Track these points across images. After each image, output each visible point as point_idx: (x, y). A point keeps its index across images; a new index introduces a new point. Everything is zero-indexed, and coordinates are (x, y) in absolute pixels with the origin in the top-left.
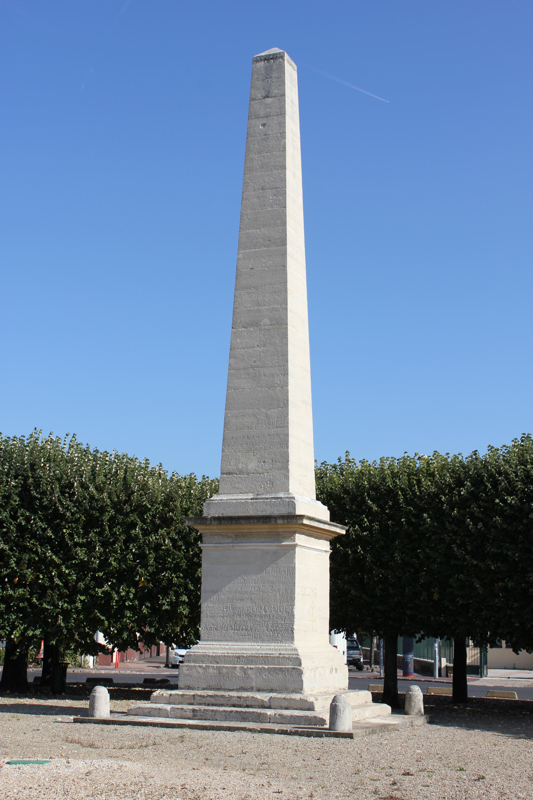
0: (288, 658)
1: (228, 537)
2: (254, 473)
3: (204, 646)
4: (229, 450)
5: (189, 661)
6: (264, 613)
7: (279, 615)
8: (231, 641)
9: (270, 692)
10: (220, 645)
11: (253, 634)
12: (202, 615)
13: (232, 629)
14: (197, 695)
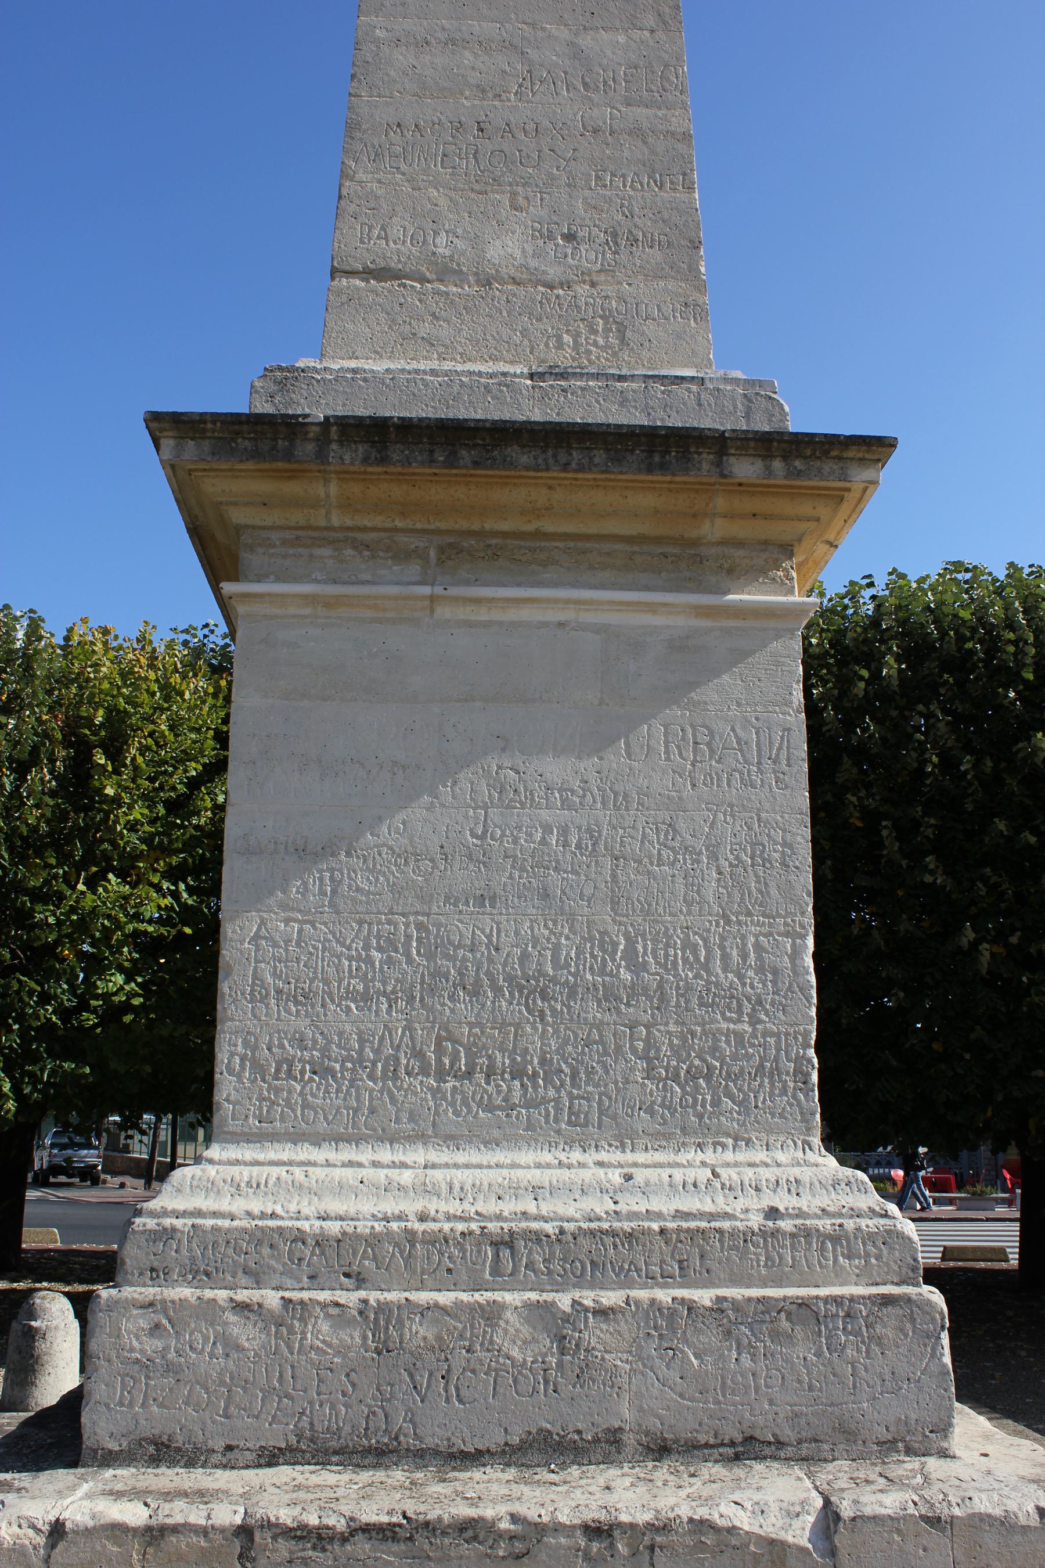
0: (837, 1238)
1: (403, 556)
2: (515, 281)
3: (246, 1171)
4: (380, 176)
5: (157, 1274)
6: (625, 975)
7: (717, 984)
8: (419, 1138)
9: (737, 1457)
10: (351, 1164)
11: (557, 1100)
12: (224, 987)
13: (425, 1071)
14: (267, 1525)
